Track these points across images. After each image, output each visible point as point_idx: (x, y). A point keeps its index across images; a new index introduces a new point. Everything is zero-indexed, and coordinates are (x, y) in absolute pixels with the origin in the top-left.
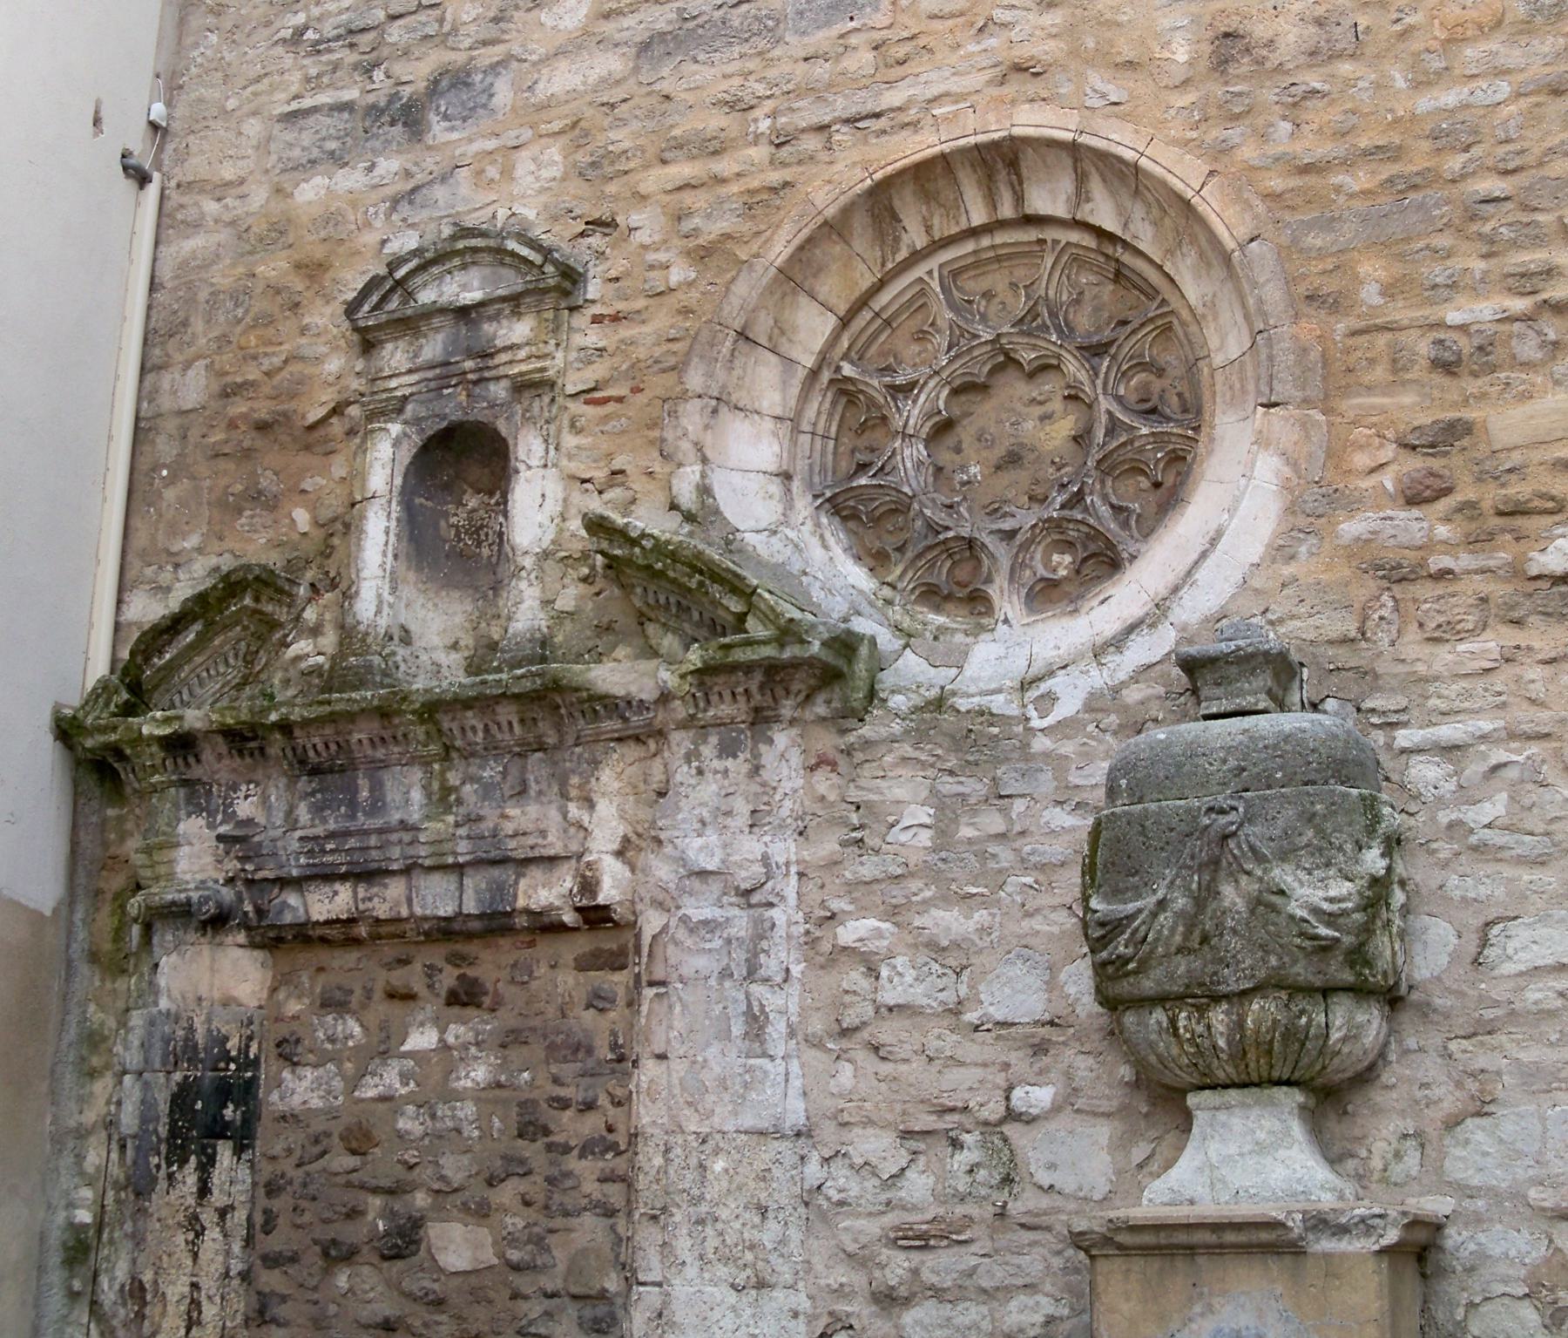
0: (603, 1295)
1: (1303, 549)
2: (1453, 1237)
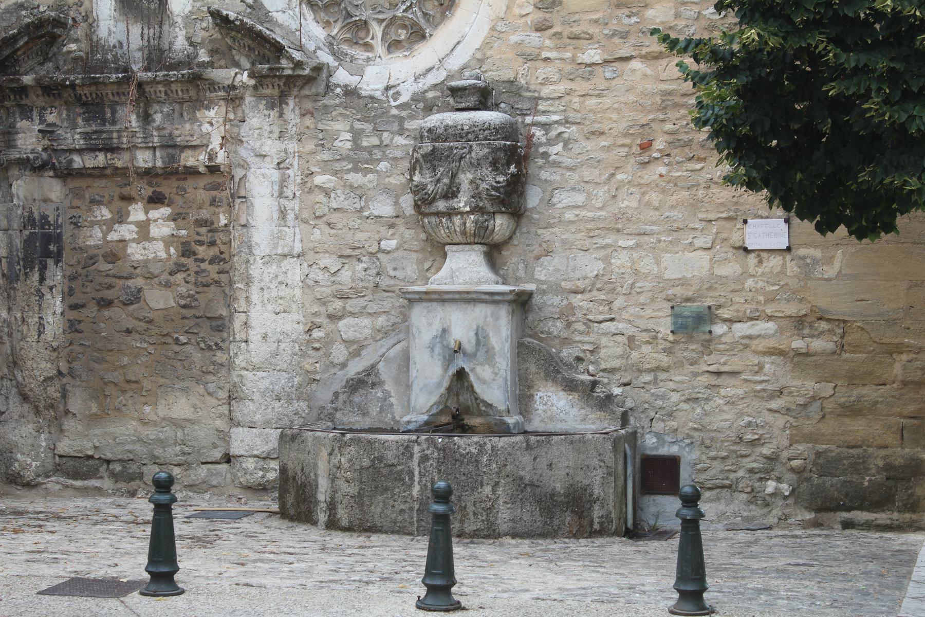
0: (221, 317)
1: (496, 44)
2: (537, 300)
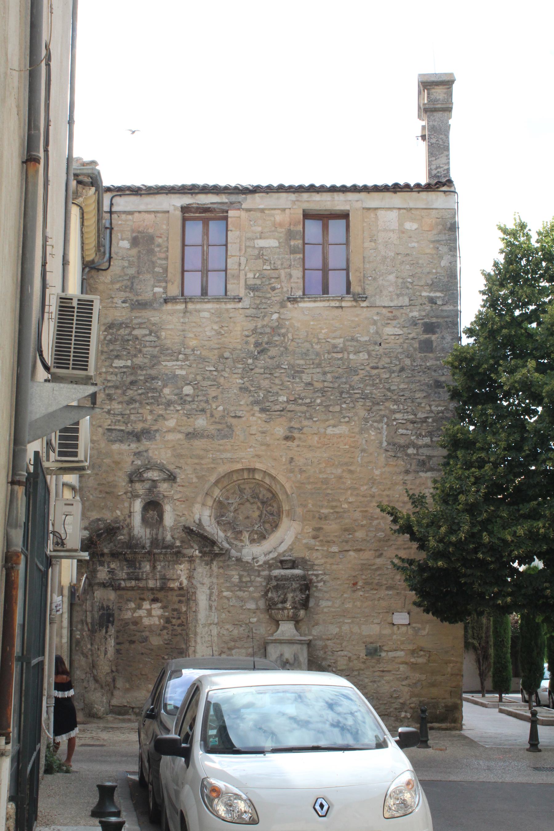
0: (182, 648)
2: (313, 642)
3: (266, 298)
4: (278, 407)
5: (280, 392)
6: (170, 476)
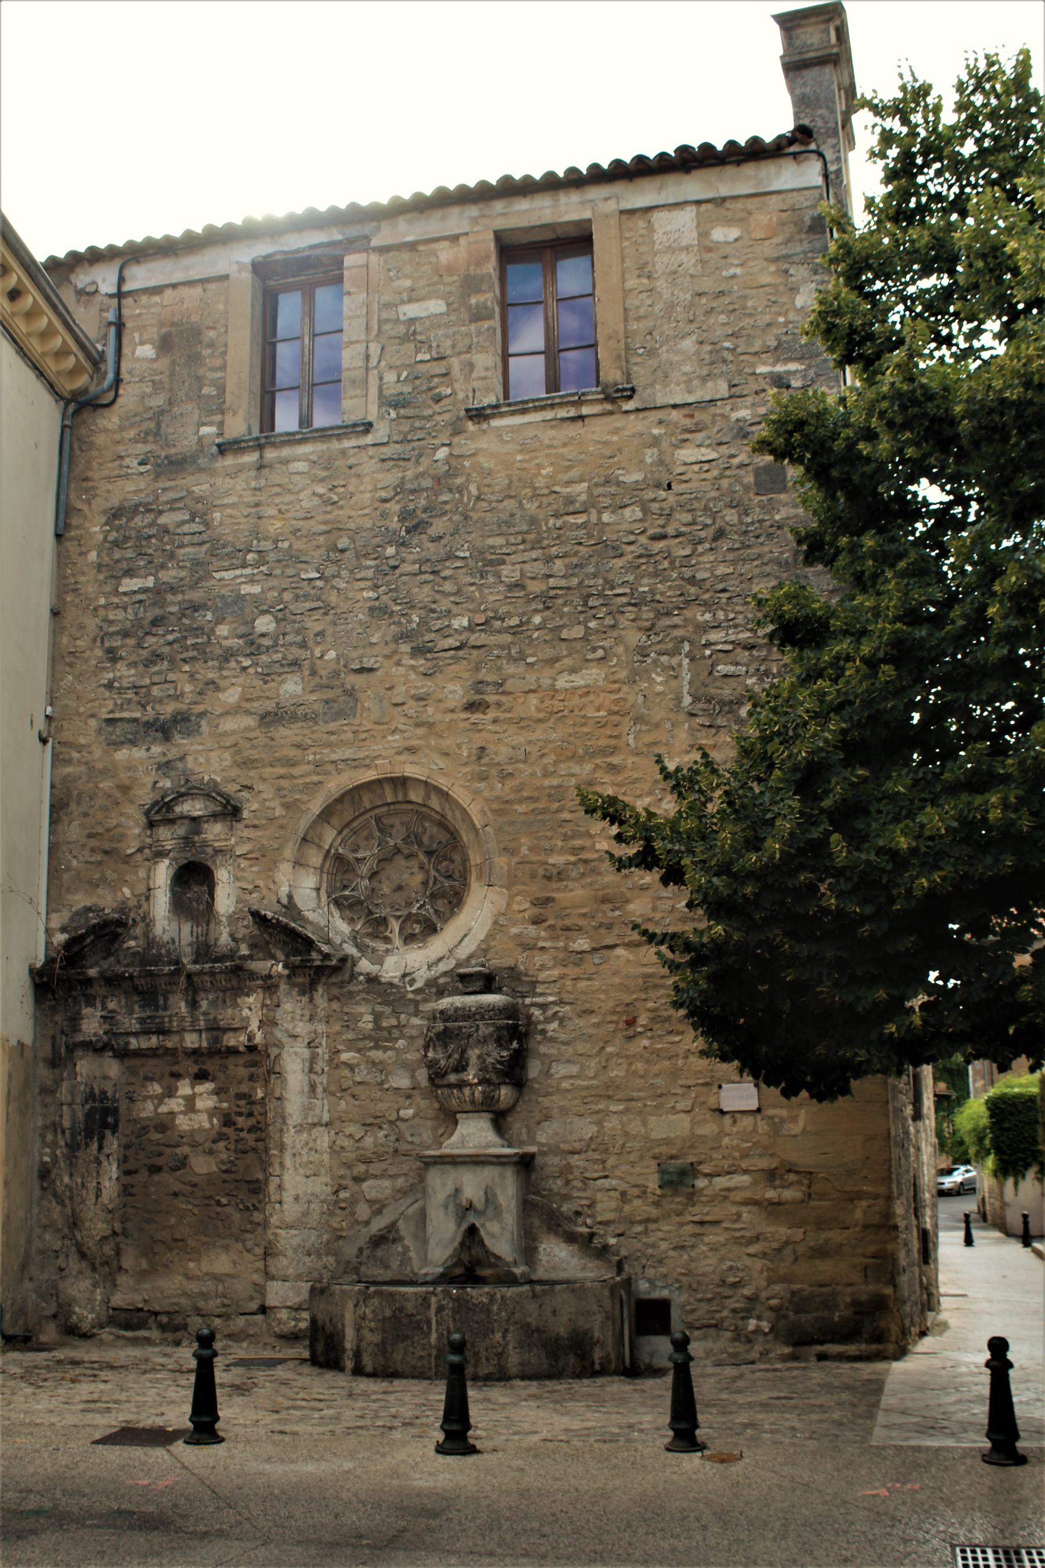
0: (257, 1181)
2: (539, 1160)
3: (423, 418)
4: (451, 642)
5: (455, 609)
6: (225, 807)
